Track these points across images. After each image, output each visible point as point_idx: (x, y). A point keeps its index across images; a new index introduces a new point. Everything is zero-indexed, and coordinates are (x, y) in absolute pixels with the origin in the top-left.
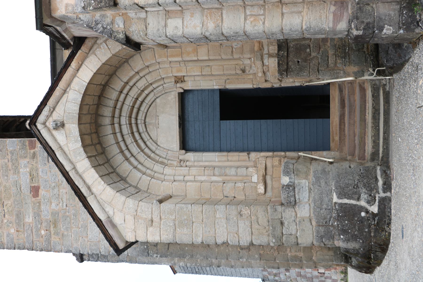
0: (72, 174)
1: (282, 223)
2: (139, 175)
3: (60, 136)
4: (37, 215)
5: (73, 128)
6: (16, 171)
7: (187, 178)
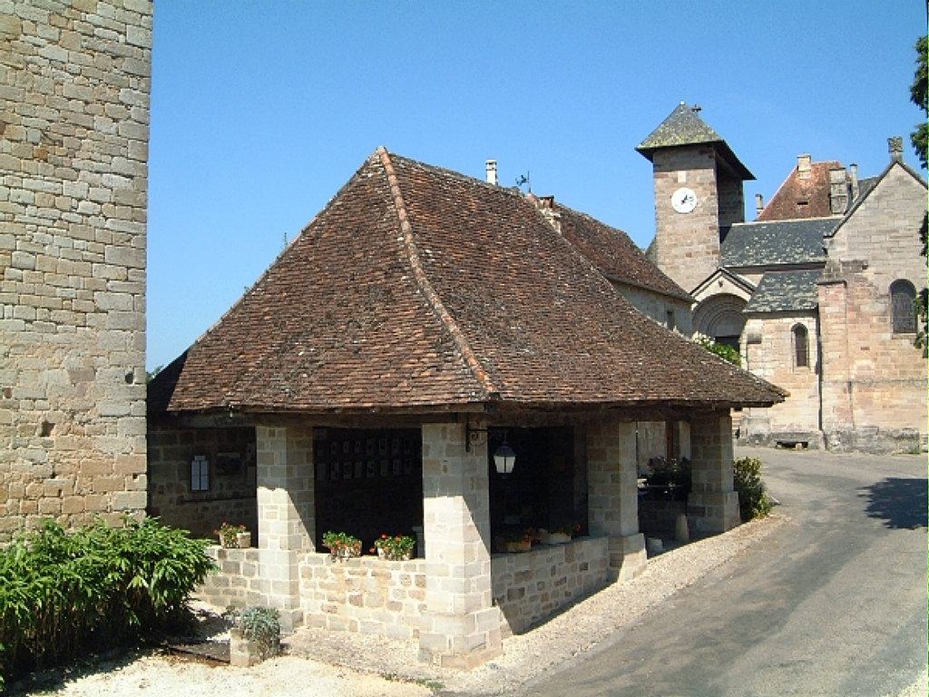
0: (698, 291)
3: (716, 283)
5: (720, 291)
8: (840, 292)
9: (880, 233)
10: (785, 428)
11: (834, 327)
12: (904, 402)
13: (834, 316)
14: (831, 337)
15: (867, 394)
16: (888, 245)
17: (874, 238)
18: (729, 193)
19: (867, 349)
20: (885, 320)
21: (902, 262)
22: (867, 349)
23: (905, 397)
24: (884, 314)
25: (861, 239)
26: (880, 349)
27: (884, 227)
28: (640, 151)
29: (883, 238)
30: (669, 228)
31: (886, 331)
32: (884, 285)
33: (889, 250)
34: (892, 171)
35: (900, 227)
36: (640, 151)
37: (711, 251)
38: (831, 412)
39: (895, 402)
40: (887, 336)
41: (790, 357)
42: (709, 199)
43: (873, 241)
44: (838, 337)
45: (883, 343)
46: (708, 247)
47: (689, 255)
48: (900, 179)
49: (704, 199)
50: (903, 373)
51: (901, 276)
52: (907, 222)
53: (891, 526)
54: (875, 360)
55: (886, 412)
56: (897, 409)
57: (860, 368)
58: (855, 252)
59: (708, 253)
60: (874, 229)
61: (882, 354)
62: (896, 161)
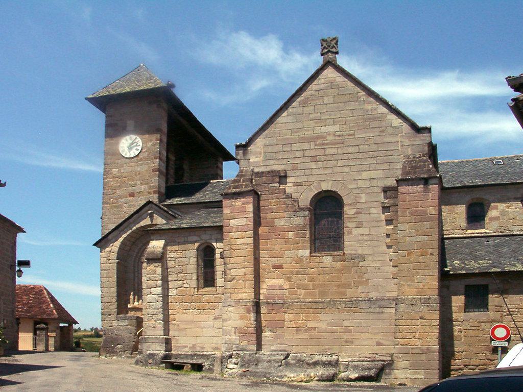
1: (110, 315)
2: (136, 251)
4: (121, 197)
6: (142, 184)
7: (136, 273)
8: (248, 203)
9: (303, 140)
10: (187, 349)
11: (239, 241)
12: (323, 325)
13: (238, 229)
14: (235, 253)
15: (278, 317)
16: (313, 153)
17: (296, 147)
18: (207, 168)
19: (279, 267)
20: (305, 235)
21: (329, 171)
22: (279, 267)
23: (322, 321)
24: (302, 228)
25: (279, 148)
26: (296, 267)
27: (308, 134)
28: (87, 99)
29: (306, 146)
30: (115, 171)
31: (304, 248)
32: (305, 198)
33: (314, 159)
34: (325, 72)
35: (328, 133)
36: (87, 99)
37: (152, 191)
38: (233, 334)
39: (310, 325)
40: (306, 253)
41: (195, 277)
42: (154, 145)
43: (294, 149)
44: (243, 252)
45: (300, 260)
46: (150, 188)
47: (132, 195)
48: (332, 84)
49: (149, 144)
50: (322, 294)
51: (325, 187)
52: (337, 128)
53: (511, 107)
54: (289, 279)
55: (300, 336)
56: (313, 333)
57: (272, 288)
58: (271, 162)
59: (150, 193)
60: (296, 136)
61: (298, 273)
62: (328, 64)
